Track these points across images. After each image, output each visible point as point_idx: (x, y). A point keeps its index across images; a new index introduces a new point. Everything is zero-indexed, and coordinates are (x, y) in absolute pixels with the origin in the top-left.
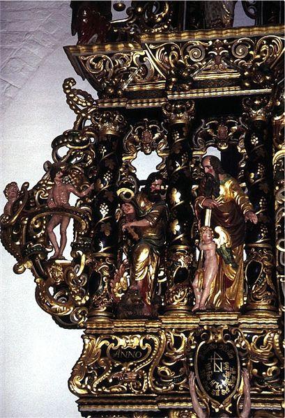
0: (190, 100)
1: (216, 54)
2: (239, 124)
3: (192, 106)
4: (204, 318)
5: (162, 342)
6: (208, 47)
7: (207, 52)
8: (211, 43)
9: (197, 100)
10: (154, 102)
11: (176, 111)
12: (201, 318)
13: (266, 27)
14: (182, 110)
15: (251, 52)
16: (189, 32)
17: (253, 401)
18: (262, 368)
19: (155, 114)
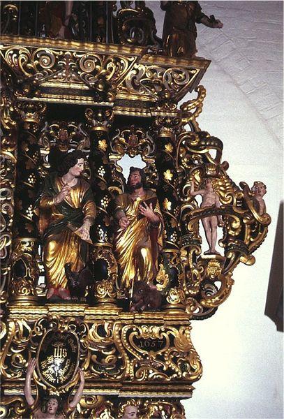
0: (42, 103)
1: (65, 63)
2: (78, 130)
3: (43, 107)
4: (15, 312)
5: (10, 333)
6: (59, 56)
7: (57, 60)
8: (61, 53)
9: (48, 103)
10: (147, 112)
11: (26, 110)
12: (50, 310)
13: (30, 38)
14: (32, 110)
15: (98, 67)
16: (94, 44)
17: (85, 388)
18: (101, 356)
19: (147, 124)
